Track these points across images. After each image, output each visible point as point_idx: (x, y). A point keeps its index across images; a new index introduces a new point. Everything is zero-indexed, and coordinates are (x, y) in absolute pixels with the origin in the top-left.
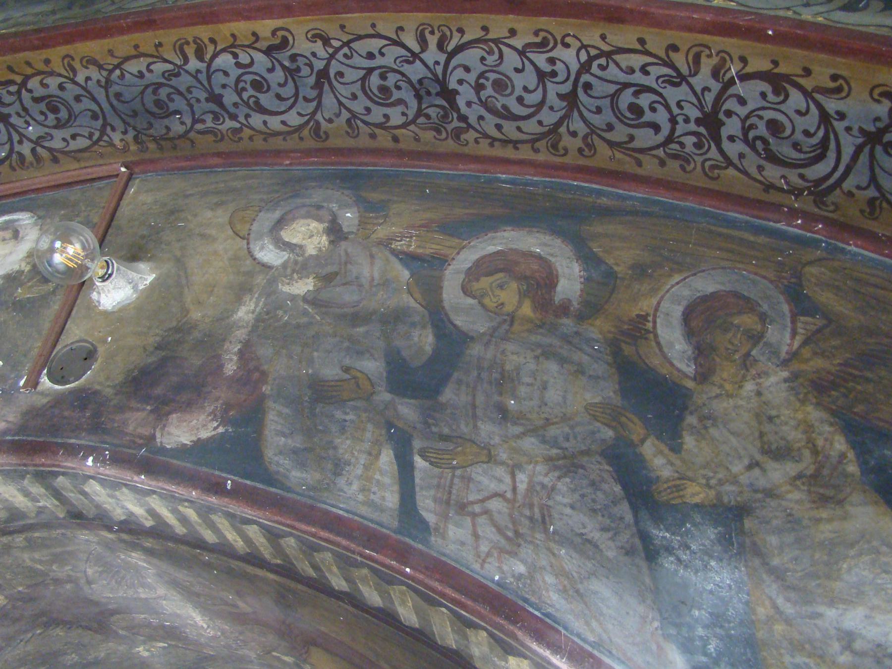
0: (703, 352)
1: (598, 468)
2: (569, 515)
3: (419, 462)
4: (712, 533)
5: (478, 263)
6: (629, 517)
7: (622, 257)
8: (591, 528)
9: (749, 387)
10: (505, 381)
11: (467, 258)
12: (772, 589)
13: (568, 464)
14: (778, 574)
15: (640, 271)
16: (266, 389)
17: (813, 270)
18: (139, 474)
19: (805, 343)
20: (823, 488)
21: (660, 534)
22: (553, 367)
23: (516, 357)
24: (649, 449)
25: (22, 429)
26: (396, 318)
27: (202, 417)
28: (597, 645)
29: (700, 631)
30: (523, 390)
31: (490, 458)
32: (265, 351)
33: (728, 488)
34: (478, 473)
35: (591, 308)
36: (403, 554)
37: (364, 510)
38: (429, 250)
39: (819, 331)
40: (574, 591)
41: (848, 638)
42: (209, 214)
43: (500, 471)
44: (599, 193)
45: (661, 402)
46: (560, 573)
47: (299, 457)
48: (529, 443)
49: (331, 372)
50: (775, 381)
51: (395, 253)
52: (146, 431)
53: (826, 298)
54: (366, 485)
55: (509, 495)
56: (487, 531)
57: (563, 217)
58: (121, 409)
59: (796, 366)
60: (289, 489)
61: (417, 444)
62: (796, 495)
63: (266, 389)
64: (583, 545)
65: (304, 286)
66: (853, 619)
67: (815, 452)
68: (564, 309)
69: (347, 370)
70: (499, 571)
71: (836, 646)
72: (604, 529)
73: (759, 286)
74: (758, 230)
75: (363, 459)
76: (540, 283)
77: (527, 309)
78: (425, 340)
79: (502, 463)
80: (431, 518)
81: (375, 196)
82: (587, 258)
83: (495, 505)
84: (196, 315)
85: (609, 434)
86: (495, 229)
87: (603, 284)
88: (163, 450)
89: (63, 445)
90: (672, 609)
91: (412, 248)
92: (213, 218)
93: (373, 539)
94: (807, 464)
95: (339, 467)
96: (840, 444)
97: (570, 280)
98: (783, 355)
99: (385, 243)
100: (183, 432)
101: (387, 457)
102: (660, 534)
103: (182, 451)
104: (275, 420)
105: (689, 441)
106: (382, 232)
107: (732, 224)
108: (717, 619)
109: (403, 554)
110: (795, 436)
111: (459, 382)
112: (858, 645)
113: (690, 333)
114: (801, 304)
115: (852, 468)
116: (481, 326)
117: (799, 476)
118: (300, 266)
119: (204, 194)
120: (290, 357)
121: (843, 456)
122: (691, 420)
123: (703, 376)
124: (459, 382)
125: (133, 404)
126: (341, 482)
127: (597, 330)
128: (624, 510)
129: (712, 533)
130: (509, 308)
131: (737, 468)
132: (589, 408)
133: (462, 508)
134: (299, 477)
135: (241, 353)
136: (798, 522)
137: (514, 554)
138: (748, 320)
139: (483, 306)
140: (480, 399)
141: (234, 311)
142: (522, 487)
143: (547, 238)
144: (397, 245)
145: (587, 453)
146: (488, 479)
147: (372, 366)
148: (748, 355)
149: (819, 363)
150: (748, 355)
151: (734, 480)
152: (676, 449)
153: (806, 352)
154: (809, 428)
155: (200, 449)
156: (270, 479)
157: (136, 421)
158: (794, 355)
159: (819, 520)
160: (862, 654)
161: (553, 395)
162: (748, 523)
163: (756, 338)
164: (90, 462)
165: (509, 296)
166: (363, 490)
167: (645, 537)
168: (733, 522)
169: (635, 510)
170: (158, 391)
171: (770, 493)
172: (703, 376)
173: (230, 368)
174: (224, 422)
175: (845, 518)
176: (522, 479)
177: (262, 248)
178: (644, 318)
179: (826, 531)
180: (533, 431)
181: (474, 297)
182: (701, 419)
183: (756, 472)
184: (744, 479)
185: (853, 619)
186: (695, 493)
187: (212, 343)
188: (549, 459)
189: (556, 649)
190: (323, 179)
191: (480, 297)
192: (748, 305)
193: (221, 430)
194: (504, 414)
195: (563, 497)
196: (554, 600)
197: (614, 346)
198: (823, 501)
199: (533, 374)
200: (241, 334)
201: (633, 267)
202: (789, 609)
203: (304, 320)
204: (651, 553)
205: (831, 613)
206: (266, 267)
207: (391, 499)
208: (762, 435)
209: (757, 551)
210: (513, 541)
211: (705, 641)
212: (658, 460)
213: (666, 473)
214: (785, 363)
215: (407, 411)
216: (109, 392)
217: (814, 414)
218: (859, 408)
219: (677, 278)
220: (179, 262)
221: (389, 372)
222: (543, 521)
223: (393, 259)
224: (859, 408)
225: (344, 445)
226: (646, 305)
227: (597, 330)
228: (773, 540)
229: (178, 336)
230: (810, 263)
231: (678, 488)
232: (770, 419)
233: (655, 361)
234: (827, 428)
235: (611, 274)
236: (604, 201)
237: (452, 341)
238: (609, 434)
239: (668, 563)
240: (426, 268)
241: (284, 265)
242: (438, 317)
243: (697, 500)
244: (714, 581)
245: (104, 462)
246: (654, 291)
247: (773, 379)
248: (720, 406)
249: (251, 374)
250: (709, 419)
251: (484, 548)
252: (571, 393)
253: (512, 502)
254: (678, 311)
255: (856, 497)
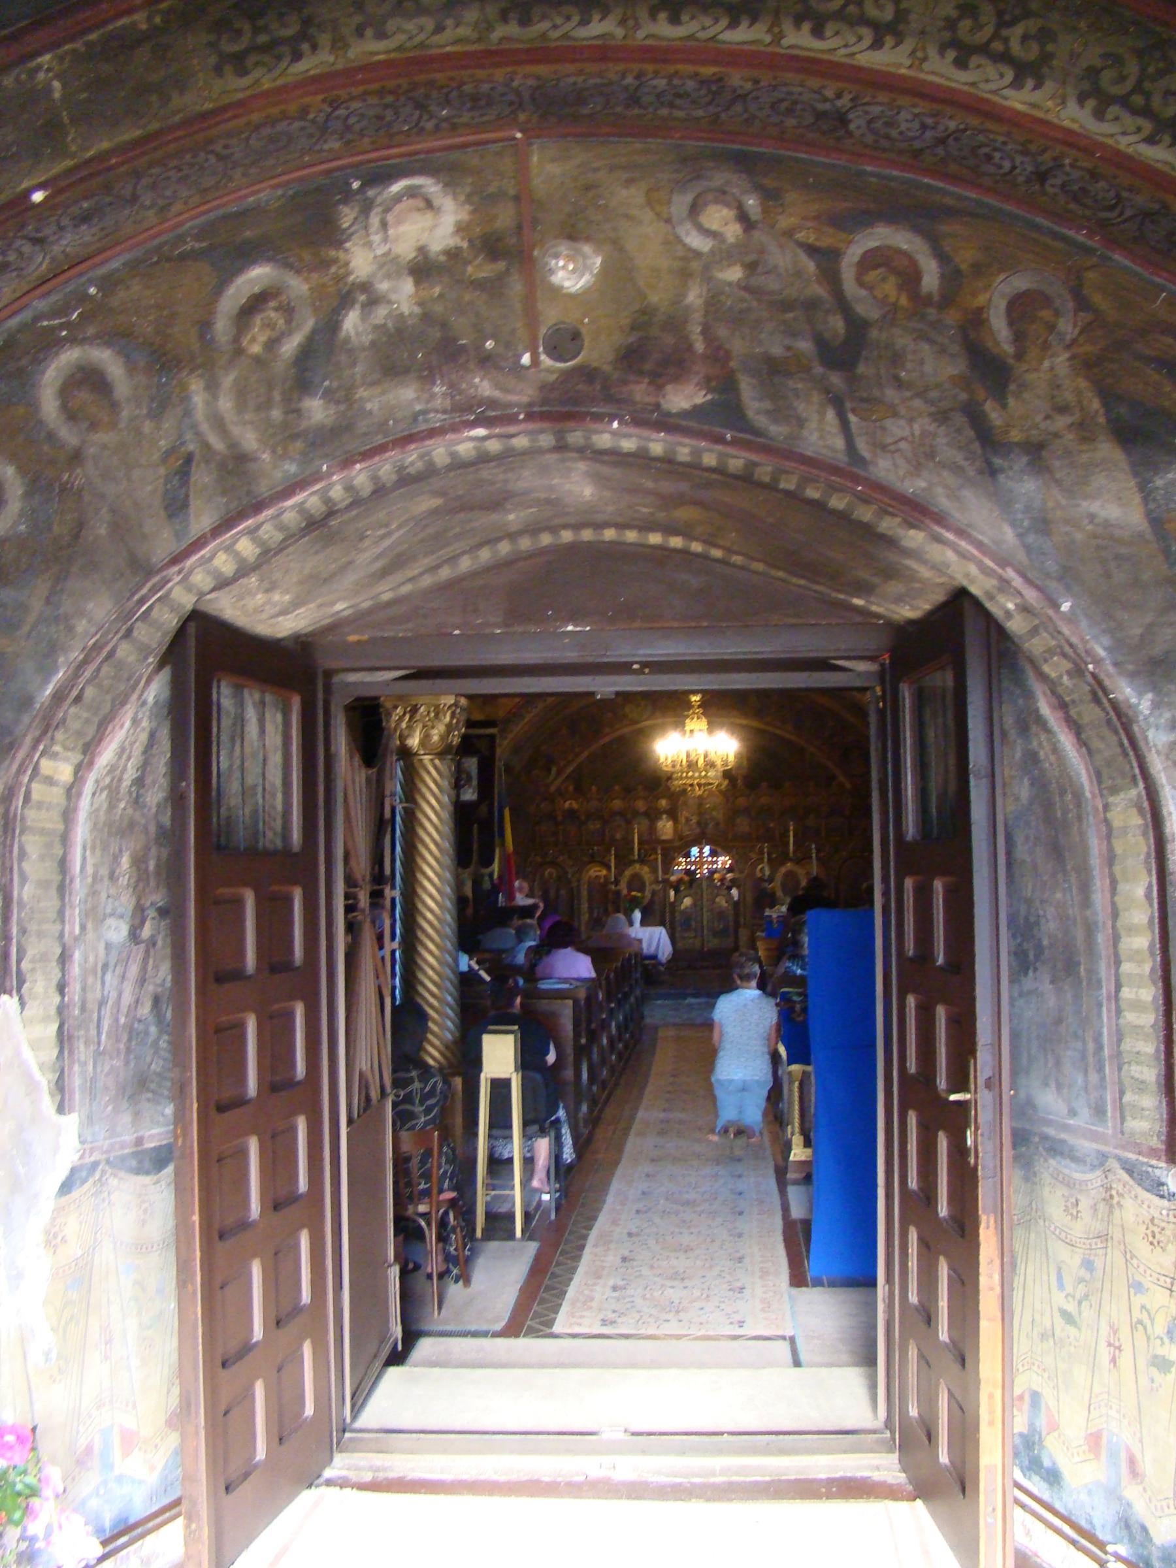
0: (1019, 337)
1: (960, 419)
2: (948, 453)
3: (852, 418)
4: (1025, 459)
5: (866, 255)
6: (979, 451)
7: (966, 257)
8: (959, 458)
9: (1046, 364)
10: (897, 359)
11: (853, 254)
12: (1055, 492)
13: (942, 417)
14: (1058, 483)
15: (978, 269)
16: (732, 364)
17: (1090, 275)
18: (659, 431)
19: (1081, 333)
20: (1085, 431)
21: (998, 461)
22: (926, 347)
23: (902, 340)
24: (988, 406)
25: (545, 401)
26: (811, 306)
27: (691, 387)
28: (969, 525)
29: (1020, 516)
30: (909, 365)
31: (895, 415)
32: (722, 332)
33: (1034, 432)
34: (889, 423)
35: (947, 300)
36: (856, 479)
37: (824, 451)
38: (825, 242)
39: (1090, 324)
40: (954, 496)
41: (1092, 517)
42: (624, 193)
43: (902, 422)
44: (944, 192)
45: (991, 371)
46: (946, 487)
47: (776, 415)
48: (917, 403)
49: (777, 351)
50: (1061, 360)
51: (801, 245)
52: (650, 399)
53: (1097, 299)
54: (821, 434)
55: (910, 439)
56: (901, 462)
57: (919, 214)
58: (625, 383)
59: (1075, 350)
60: (771, 439)
61: (848, 405)
62: (1070, 437)
63: (732, 364)
64: (957, 469)
65: (734, 274)
66: (1095, 507)
67: (1082, 409)
68: (928, 301)
69: (788, 348)
70: (913, 486)
71: (1086, 521)
72: (966, 459)
73: (1058, 290)
74: (1056, 236)
75: (815, 417)
76: (910, 278)
77: (904, 301)
78: (837, 325)
79: (903, 417)
80: (866, 454)
81: (768, 182)
82: (942, 257)
83: (903, 445)
84: (654, 298)
85: (964, 396)
86: (871, 225)
87: (953, 278)
88: (669, 414)
89: (588, 413)
90: (1004, 502)
91: (811, 241)
92: (629, 197)
93: (835, 470)
94: (1076, 417)
95: (801, 423)
96: (1096, 404)
97: (931, 278)
98: (1068, 342)
99: (789, 233)
100: (682, 398)
101: (830, 415)
102: (998, 461)
103: (685, 414)
104: (747, 389)
105: (1011, 402)
106: (784, 222)
107: (1038, 228)
108: (1027, 509)
109: (856, 479)
110: (1069, 397)
111: (866, 359)
112: (1096, 521)
113: (1011, 323)
114: (1082, 303)
115: (1101, 420)
116: (874, 314)
117: (1072, 424)
118: (725, 254)
119: (612, 169)
120: (743, 338)
121: (1097, 412)
122: (1012, 387)
123: (1020, 356)
124: (866, 359)
125: (632, 378)
126: (805, 433)
127: (952, 317)
128: (976, 446)
129: (1025, 459)
130: (892, 299)
131: (1039, 418)
132: (952, 378)
133: (884, 447)
134: (777, 430)
135: (703, 333)
136: (1070, 452)
137: (919, 476)
138: (1046, 314)
139: (874, 297)
140: (883, 371)
141: (685, 296)
142: (917, 433)
143: (909, 235)
144: (800, 236)
145: (951, 410)
146: (897, 428)
147: (805, 346)
148: (1045, 341)
149: (1088, 348)
150: (1045, 341)
151: (1036, 427)
152: (1004, 406)
153: (1081, 340)
154: (1078, 392)
155: (697, 412)
156: (757, 432)
157: (640, 391)
158: (1074, 341)
159: (1081, 451)
160: (1098, 525)
161: (928, 368)
162: (1044, 453)
163: (1051, 327)
164: (615, 425)
165: (890, 288)
166: (821, 437)
167: (989, 464)
168: (1036, 452)
169: (983, 446)
170: (647, 366)
171: (1056, 435)
172: (1020, 356)
173: (700, 347)
174: (710, 390)
175: (1095, 450)
176: (916, 426)
177: (687, 234)
178: (980, 310)
179: (1084, 458)
180: (918, 395)
181: (866, 288)
182: (1020, 386)
183: (1048, 422)
184: (1043, 426)
185: (1095, 507)
186: (1016, 436)
187: (675, 323)
188: (930, 415)
189: (948, 528)
190: (720, 158)
191: (870, 288)
192: (1046, 300)
193: (709, 397)
194: (899, 384)
195: (941, 441)
196: (943, 502)
197: (963, 330)
198: (1084, 440)
199: (915, 352)
200: (697, 317)
201: (972, 266)
202: (1064, 502)
203: (745, 305)
204: (992, 472)
205: (1085, 504)
206: (697, 254)
207: (839, 443)
208: (1053, 397)
209: (1048, 470)
210: (917, 468)
211: (1022, 520)
212: (994, 414)
213: (998, 423)
214: (1068, 347)
215: (836, 380)
216: (607, 368)
217: (1082, 383)
218: (1110, 380)
219: (1002, 277)
220: (617, 244)
221: (381, 721)
222: (931, 455)
223: (799, 251)
224: (1110, 380)
225: (801, 407)
226: (981, 299)
227: (952, 317)
228: (1057, 463)
229: (646, 318)
230: (1087, 269)
231: (1007, 432)
232: (1058, 386)
233: (990, 344)
234: (1090, 394)
235: (958, 272)
236: (948, 201)
237: (858, 327)
238: (964, 396)
239: (1001, 478)
240: (827, 259)
241: (712, 252)
242: (843, 305)
243: (1016, 440)
244: (1026, 487)
245: (627, 424)
246: (987, 288)
247: (1061, 359)
248: (1031, 377)
249: (718, 354)
250: (1023, 386)
251: (901, 473)
252: (938, 366)
253: (912, 442)
254: (1003, 305)
255: (1102, 438)
